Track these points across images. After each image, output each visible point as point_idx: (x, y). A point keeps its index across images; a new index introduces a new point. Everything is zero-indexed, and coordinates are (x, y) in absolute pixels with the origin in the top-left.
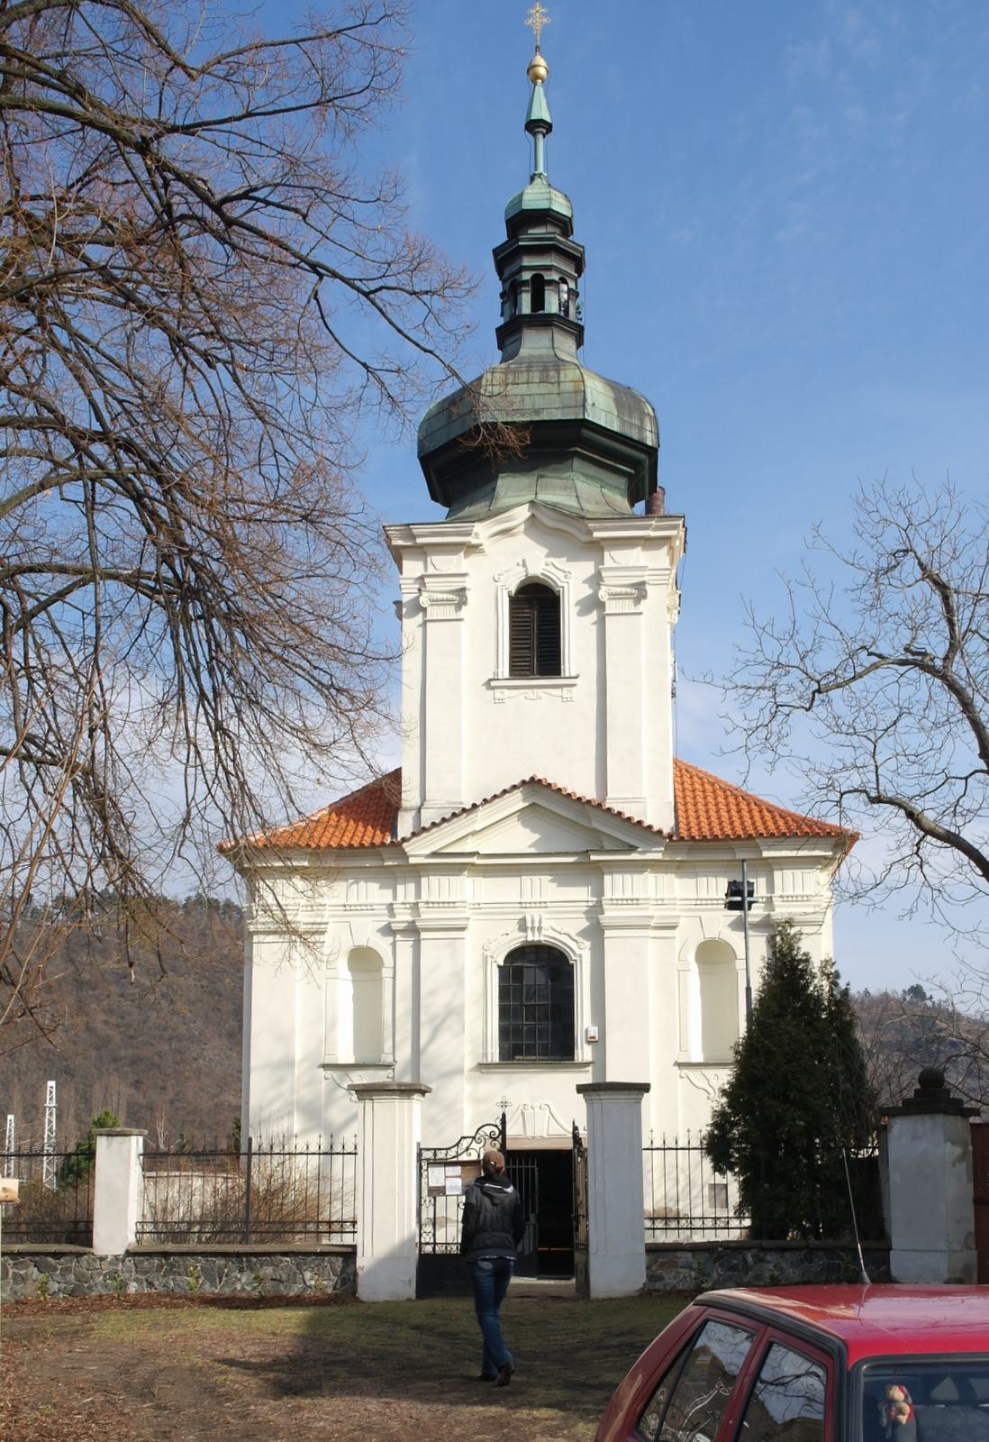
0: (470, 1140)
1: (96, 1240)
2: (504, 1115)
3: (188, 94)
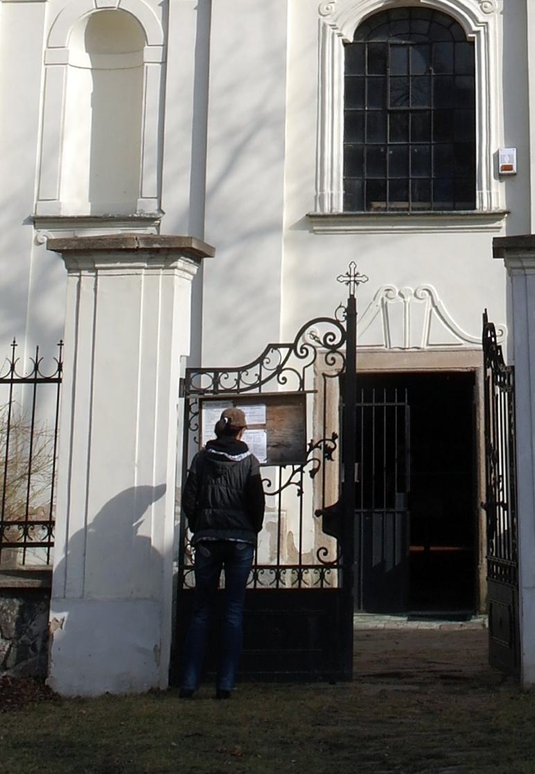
0: (284, 351)
2: (352, 300)
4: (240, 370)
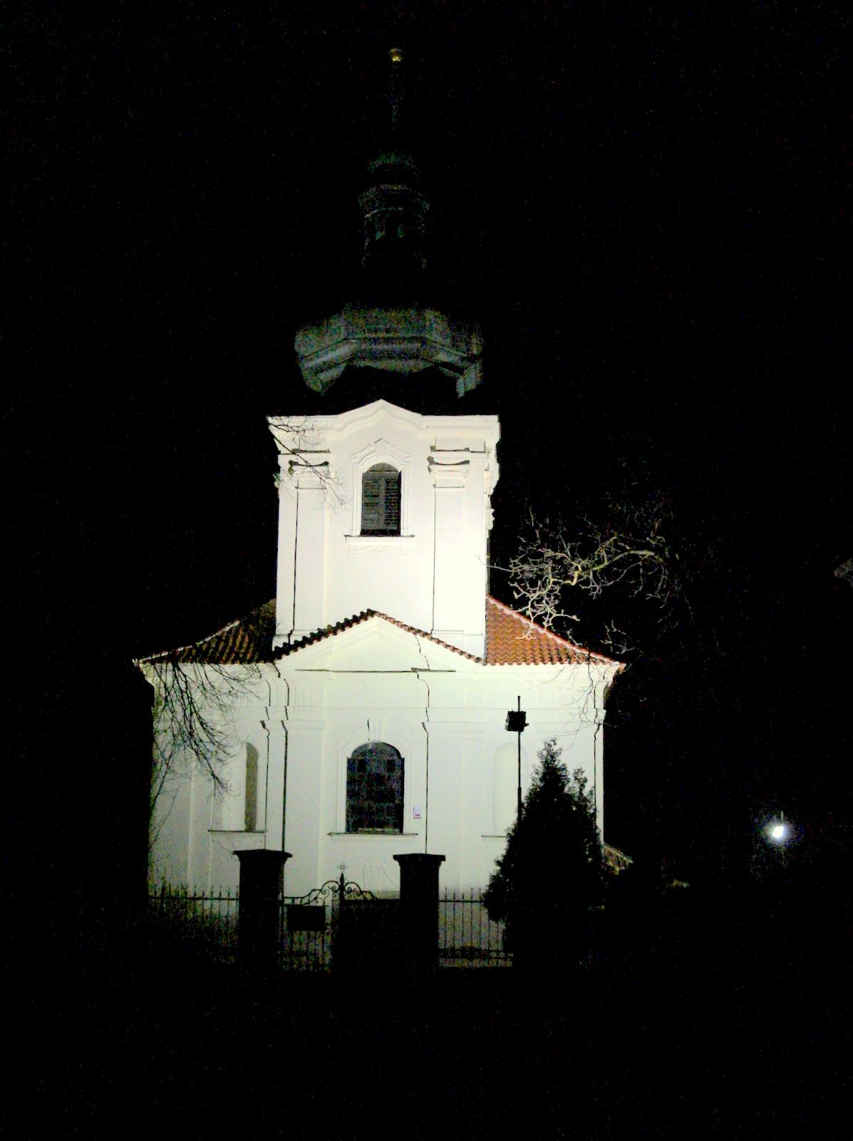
2: (342, 875)
4: (302, 898)
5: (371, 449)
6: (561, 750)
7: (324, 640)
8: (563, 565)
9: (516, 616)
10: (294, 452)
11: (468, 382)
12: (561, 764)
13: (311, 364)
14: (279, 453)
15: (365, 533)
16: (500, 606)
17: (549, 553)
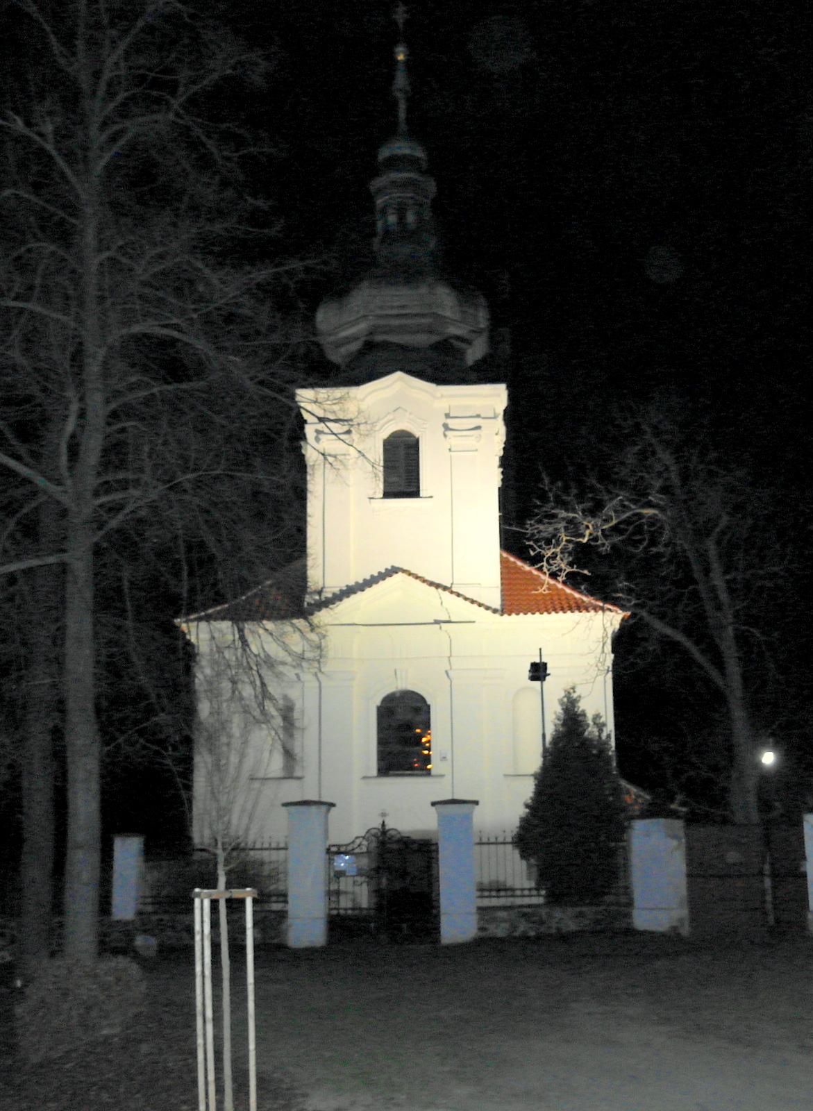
1: (114, 910)
2: (384, 822)
3: (601, 668)
5: (391, 417)
6: (580, 697)
7: (353, 597)
8: (575, 524)
9: (535, 573)
10: (321, 420)
11: (476, 352)
12: (580, 709)
13: (332, 339)
14: (305, 422)
15: (388, 494)
16: (512, 559)
17: (563, 514)
